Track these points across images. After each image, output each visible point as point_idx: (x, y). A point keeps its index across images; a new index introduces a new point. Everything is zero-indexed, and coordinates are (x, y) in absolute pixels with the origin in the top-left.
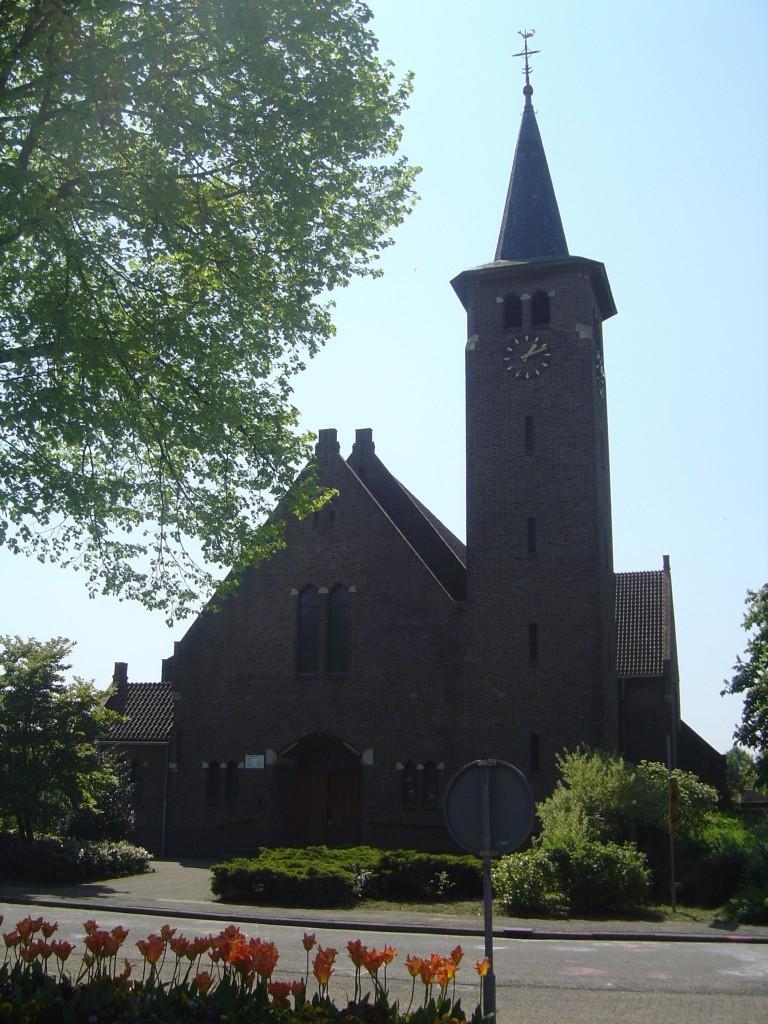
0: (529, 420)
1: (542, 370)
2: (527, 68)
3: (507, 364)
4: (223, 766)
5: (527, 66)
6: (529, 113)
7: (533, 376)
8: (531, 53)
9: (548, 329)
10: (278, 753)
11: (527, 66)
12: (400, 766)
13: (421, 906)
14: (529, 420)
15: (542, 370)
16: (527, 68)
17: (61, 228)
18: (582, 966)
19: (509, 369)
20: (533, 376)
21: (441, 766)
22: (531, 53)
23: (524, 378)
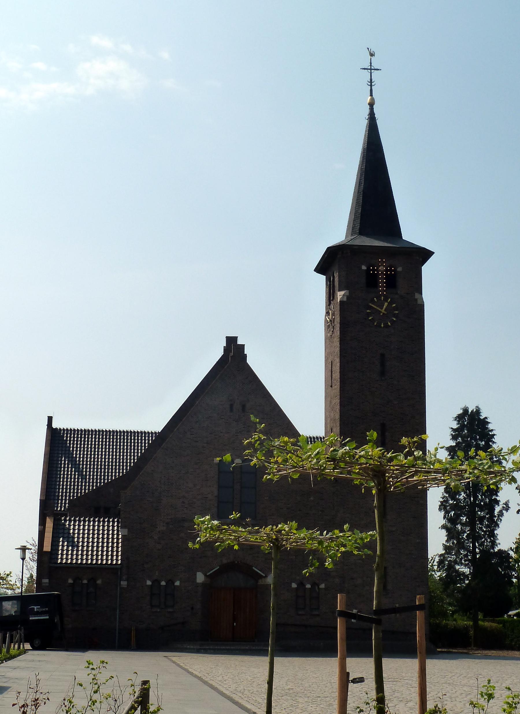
0: (383, 355)
1: (393, 322)
2: (371, 82)
3: (368, 315)
4: (163, 583)
5: (371, 79)
6: (371, 105)
7: (386, 326)
8: (371, 65)
9: (397, 294)
10: (205, 575)
11: (371, 79)
12: (294, 585)
13: (236, 656)
14: (383, 355)
15: (393, 322)
16: (371, 82)
17: (229, 463)
18: (315, 450)
19: (370, 318)
20: (386, 326)
21: (322, 586)
22: (371, 65)
23: (381, 327)
